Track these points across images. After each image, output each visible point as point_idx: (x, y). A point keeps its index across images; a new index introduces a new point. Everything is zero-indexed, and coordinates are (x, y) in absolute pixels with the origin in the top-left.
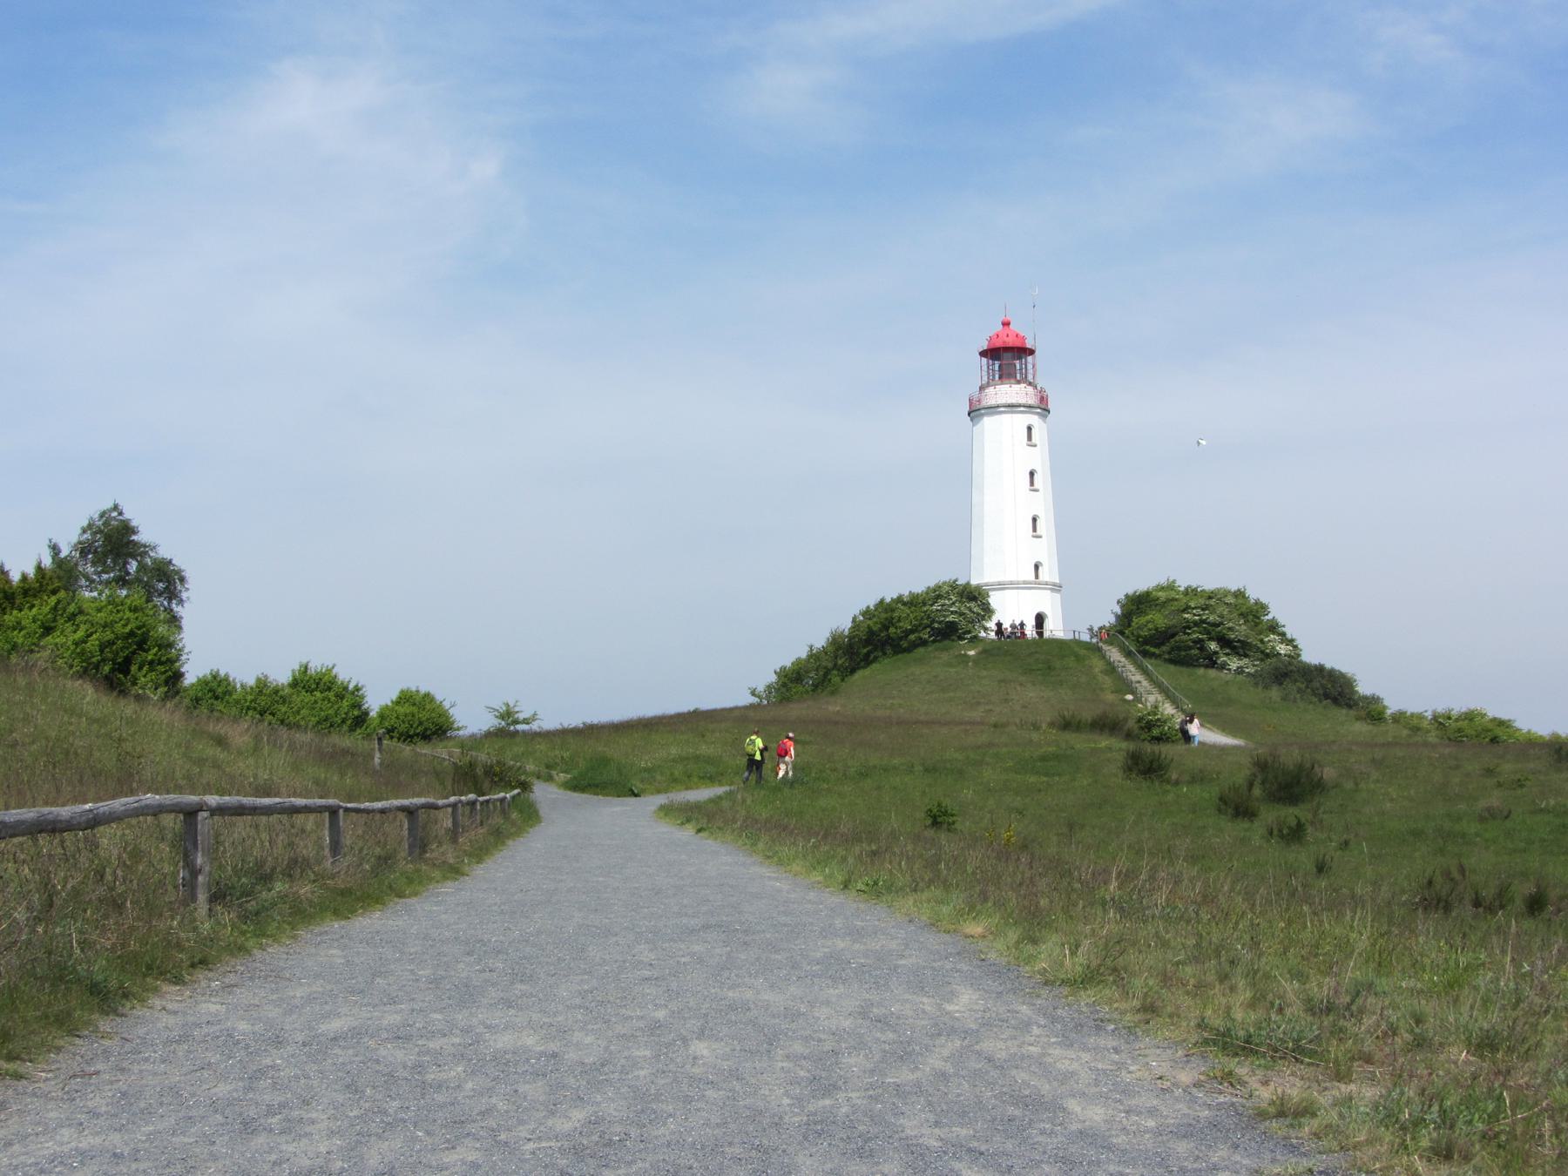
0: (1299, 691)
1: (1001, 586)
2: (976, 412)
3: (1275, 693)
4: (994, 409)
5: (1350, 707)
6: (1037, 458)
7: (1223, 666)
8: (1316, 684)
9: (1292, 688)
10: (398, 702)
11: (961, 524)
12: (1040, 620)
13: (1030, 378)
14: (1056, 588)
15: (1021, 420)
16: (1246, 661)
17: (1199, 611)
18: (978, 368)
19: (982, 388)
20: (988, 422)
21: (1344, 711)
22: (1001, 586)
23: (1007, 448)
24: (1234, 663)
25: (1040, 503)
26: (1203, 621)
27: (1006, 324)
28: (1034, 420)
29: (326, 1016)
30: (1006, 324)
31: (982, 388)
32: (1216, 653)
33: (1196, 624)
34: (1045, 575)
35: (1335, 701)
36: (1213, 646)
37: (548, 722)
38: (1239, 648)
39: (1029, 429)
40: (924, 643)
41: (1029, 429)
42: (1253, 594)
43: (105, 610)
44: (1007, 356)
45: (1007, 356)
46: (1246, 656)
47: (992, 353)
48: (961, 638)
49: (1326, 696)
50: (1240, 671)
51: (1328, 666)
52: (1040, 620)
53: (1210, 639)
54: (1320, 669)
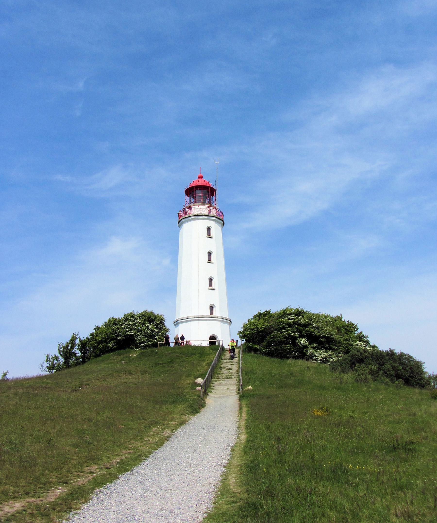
0: (371, 372)
1: (189, 319)
3: (349, 376)
5: (422, 386)
6: (216, 244)
7: (312, 357)
8: (388, 366)
9: (364, 369)
11: (169, 286)
15: (203, 224)
16: (331, 352)
17: (293, 316)
21: (417, 390)
22: (189, 319)
24: (320, 355)
25: (217, 270)
26: (295, 323)
28: (213, 224)
32: (305, 347)
33: (290, 325)
34: (216, 312)
35: (407, 382)
36: (303, 341)
38: (326, 343)
39: (209, 229)
40: (111, 350)
41: (209, 229)
43: (5, 380)
44: (201, 192)
46: (331, 349)
48: (137, 347)
49: (398, 377)
50: (325, 360)
51: (397, 351)
53: (301, 336)
54: (391, 354)
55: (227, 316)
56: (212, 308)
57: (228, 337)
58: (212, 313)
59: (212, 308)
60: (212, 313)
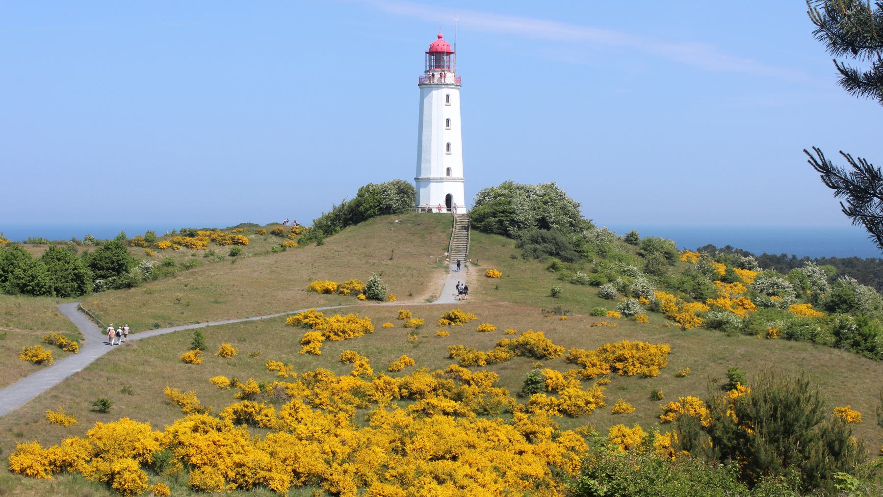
1: (428, 180)
6: (454, 112)
12: (449, 199)
18: (423, 62)
25: (455, 136)
27: (439, 37)
34: (454, 174)
39: (448, 96)
41: (448, 96)
47: (431, 53)
52: (449, 199)
56: (448, 170)
57: (462, 208)
58: (448, 174)
59: (448, 170)
60: (448, 174)
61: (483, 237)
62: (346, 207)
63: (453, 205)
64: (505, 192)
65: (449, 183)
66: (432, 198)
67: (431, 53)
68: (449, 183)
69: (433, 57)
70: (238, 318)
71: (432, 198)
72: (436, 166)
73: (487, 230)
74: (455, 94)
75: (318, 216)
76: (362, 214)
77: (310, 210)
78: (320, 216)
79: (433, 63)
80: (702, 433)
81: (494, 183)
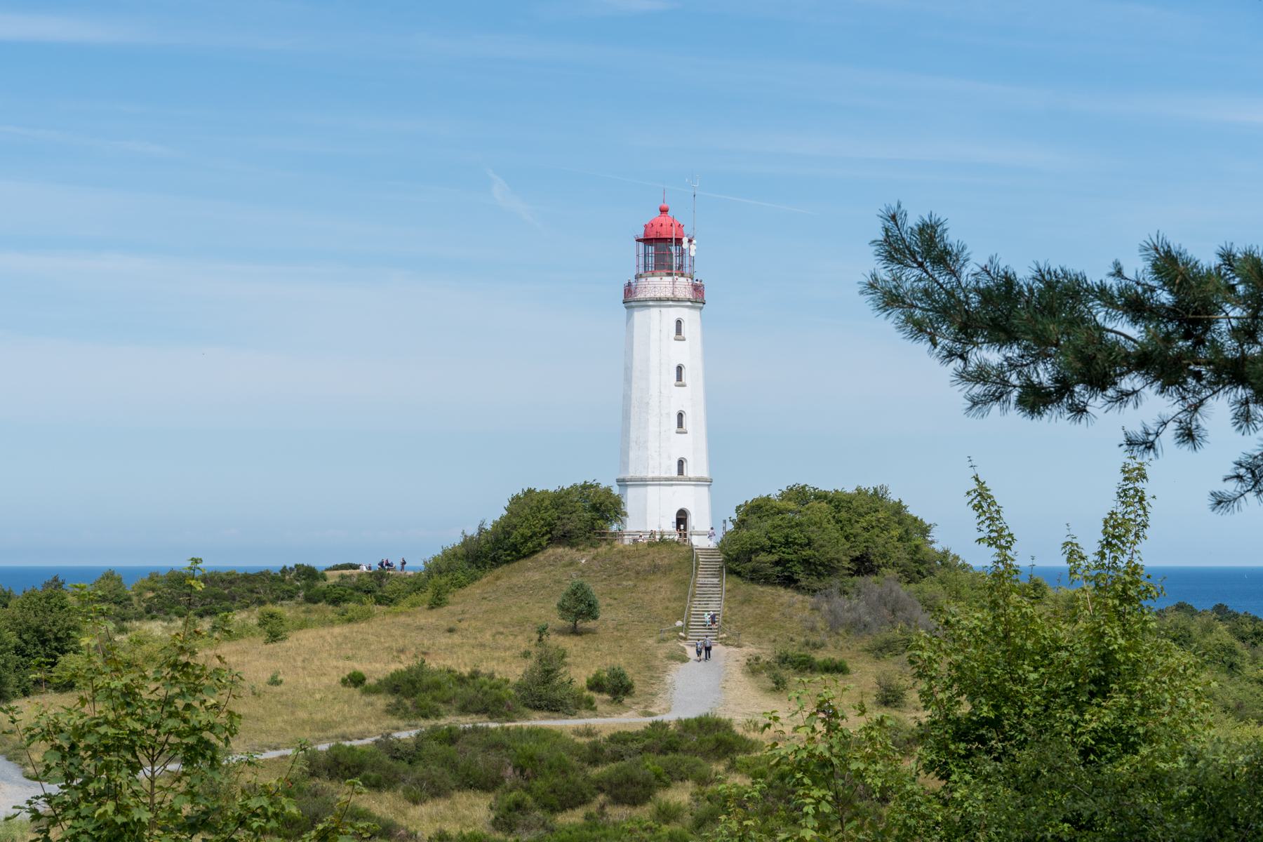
1: (643, 482)
2: (630, 298)
4: (645, 303)
6: (689, 352)
10: (741, 524)
12: (682, 518)
13: (687, 270)
14: (708, 482)
15: (672, 314)
18: (630, 256)
19: (638, 277)
20: (639, 315)
22: (643, 482)
23: (666, 341)
25: (691, 399)
27: (664, 211)
29: (398, 729)
30: (664, 211)
31: (638, 277)
34: (689, 471)
37: (416, 564)
39: (679, 323)
41: (679, 323)
42: (518, 491)
45: (661, 246)
47: (647, 241)
52: (682, 518)
55: (705, 475)
56: (681, 463)
58: (681, 471)
59: (681, 463)
60: (681, 471)
61: (745, 588)
62: (489, 527)
63: (689, 529)
64: (792, 505)
65: (677, 492)
66: (649, 514)
67: (647, 241)
68: (677, 492)
69: (651, 249)
70: (520, 731)
71: (649, 514)
72: (658, 448)
73: (756, 577)
74: (690, 316)
75: (428, 556)
76: (514, 547)
77: (418, 542)
78: (439, 552)
79: (651, 260)
80: (140, 663)
81: (770, 484)
